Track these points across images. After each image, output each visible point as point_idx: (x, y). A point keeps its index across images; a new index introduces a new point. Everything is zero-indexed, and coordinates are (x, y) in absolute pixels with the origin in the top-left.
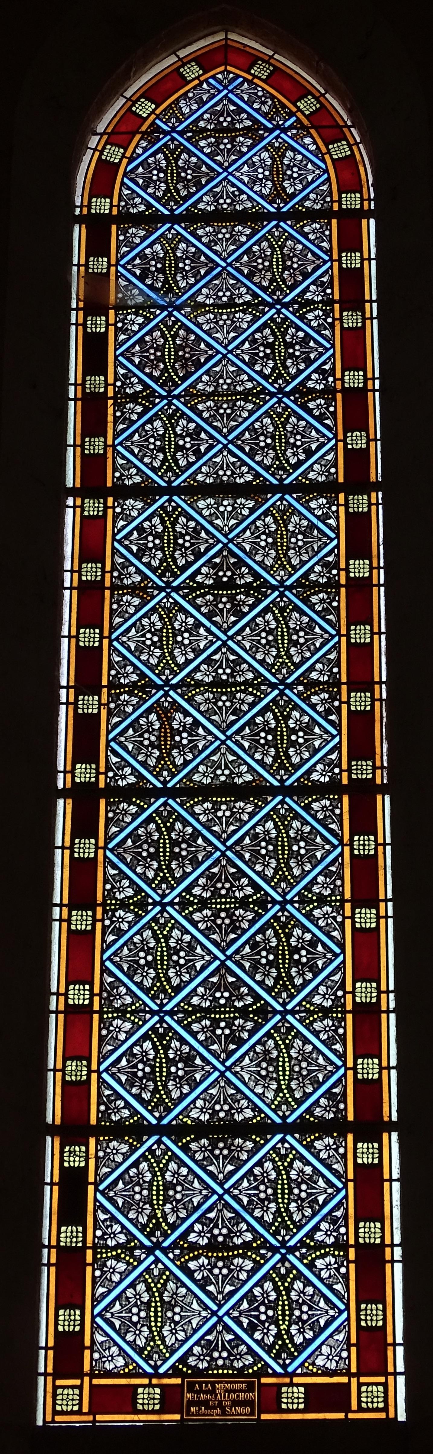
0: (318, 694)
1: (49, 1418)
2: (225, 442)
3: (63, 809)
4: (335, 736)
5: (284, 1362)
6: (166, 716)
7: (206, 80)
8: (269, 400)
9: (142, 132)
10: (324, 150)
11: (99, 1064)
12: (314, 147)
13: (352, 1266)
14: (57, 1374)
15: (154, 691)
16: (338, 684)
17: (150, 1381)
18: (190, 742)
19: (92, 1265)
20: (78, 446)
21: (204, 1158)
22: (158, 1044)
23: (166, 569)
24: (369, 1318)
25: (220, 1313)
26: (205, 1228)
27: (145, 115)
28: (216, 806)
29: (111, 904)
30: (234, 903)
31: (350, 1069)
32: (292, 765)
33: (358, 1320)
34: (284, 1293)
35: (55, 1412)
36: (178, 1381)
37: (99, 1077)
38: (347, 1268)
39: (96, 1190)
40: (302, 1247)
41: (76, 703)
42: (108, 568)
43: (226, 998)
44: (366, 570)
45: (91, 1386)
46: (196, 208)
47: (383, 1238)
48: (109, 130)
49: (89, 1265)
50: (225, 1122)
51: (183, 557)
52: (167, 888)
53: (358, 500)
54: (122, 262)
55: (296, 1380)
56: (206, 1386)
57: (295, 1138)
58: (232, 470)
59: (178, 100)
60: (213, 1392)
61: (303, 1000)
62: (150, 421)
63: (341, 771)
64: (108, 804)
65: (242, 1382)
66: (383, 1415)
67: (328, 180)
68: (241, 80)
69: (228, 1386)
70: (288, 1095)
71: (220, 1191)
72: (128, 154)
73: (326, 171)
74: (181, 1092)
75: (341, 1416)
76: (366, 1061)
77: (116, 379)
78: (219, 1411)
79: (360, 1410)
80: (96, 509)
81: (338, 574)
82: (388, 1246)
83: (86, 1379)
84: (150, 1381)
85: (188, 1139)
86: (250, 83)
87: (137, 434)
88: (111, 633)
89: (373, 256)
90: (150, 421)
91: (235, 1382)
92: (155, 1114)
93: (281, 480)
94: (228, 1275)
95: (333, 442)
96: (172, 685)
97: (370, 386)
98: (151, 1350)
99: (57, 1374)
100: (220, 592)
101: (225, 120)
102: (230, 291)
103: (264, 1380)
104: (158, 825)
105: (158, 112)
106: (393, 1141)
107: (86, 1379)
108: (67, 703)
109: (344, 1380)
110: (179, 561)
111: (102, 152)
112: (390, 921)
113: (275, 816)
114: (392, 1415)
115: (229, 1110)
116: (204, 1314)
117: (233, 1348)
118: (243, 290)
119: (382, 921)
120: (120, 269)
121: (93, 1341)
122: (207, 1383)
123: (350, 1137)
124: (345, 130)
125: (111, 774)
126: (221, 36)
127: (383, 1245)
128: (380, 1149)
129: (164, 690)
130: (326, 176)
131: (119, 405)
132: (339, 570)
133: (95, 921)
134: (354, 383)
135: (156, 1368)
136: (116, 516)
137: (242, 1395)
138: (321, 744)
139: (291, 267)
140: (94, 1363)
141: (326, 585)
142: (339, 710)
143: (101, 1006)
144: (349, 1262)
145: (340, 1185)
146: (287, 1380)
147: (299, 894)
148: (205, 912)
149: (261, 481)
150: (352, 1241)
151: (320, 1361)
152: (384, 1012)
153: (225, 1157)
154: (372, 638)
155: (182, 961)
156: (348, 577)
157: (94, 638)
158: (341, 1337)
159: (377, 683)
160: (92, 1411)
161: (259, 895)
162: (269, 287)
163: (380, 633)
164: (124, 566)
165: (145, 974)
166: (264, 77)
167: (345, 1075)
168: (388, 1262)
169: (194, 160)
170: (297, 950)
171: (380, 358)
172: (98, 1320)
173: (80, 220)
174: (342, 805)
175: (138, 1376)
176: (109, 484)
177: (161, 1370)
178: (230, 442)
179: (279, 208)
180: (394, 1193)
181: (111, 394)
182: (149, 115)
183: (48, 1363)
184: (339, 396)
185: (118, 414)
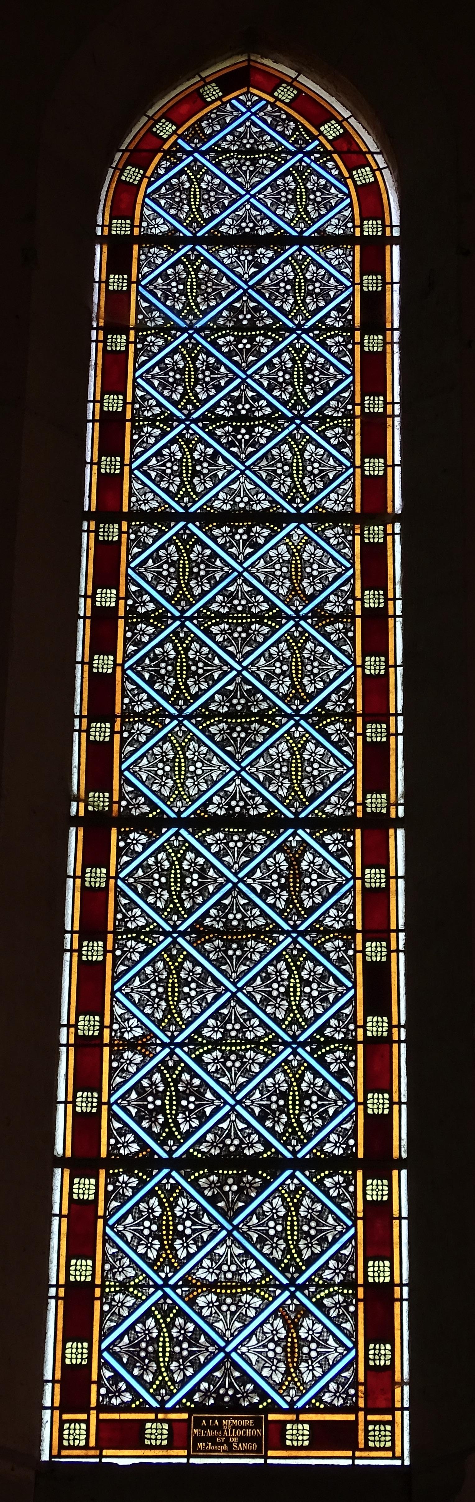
0: (334, 725)
2: (242, 468)
3: (75, 838)
4: (351, 1350)
5: (294, 1149)
7: (229, 101)
8: (289, 336)
9: (164, 151)
10: (346, 174)
11: (110, 1095)
12: (337, 172)
13: (361, 1305)
14: (64, 1408)
15: (179, 334)
16: (352, 330)
17: (156, 1416)
19: (100, 1298)
20: (100, 341)
21: (224, 640)
23: (190, 310)
25: (228, 1349)
26: (214, 1264)
27: (165, 136)
28: (229, 836)
29: (110, 1286)
31: (361, 1104)
32: (305, 1020)
33: (367, 1359)
36: (185, 1416)
37: (110, 1109)
38: (356, 1306)
39: (105, 1224)
40: (312, 932)
42: (129, 399)
43: (238, 920)
45: (99, 1421)
46: (208, 610)
48: (132, 147)
49: (97, 1299)
50: (235, 1157)
52: (189, 502)
54: (122, 875)
55: (303, 1417)
56: (213, 1422)
59: (201, 120)
60: (220, 1428)
63: (356, 804)
64: (107, 1175)
65: (249, 1419)
67: (351, 205)
68: (263, 102)
69: (235, 1422)
70: (298, 1016)
71: (232, 1102)
72: (148, 174)
73: (349, 196)
74: (185, 1374)
78: (225, 1447)
81: (354, 604)
83: (93, 1413)
84: (156, 1416)
85: (204, 832)
86: (273, 105)
88: (124, 662)
91: (242, 1418)
93: (294, 1153)
95: (353, 1106)
96: (177, 1043)
97: (389, 411)
99: (64, 1408)
100: (231, 830)
102: (248, 496)
103: (272, 1417)
104: (189, 177)
106: (401, 1178)
107: (93, 1413)
109: (352, 1417)
110: (191, 688)
112: (405, 1304)
117: (245, 1021)
118: (262, 496)
119: (396, 1108)
120: (120, 883)
121: (100, 1376)
122: (214, 1419)
123: (360, 1174)
124: (369, 156)
129: (172, 937)
130: (348, 201)
131: (116, 1054)
132: (355, 599)
135: (163, 1403)
136: (136, 351)
137: (249, 1432)
139: (312, 380)
141: (343, 1041)
143: (111, 1038)
144: (358, 1300)
145: (350, 1223)
149: (272, 1153)
150: (361, 1281)
151: (327, 1398)
152: (392, 715)
153: (233, 1314)
154: (385, 471)
155: (192, 1106)
156: (363, 608)
159: (391, 616)
161: (269, 1153)
162: (289, 401)
163: (400, 1103)
164: (122, 1133)
165: (156, 1006)
166: (287, 101)
167: (356, 1110)
168: (397, 1300)
169: (201, 861)
170: (307, 1096)
172: (106, 1355)
176: (125, 509)
177: (169, 1405)
178: (248, 468)
180: (402, 1232)
181: (106, 1039)
182: (170, 137)
183: (59, 1311)
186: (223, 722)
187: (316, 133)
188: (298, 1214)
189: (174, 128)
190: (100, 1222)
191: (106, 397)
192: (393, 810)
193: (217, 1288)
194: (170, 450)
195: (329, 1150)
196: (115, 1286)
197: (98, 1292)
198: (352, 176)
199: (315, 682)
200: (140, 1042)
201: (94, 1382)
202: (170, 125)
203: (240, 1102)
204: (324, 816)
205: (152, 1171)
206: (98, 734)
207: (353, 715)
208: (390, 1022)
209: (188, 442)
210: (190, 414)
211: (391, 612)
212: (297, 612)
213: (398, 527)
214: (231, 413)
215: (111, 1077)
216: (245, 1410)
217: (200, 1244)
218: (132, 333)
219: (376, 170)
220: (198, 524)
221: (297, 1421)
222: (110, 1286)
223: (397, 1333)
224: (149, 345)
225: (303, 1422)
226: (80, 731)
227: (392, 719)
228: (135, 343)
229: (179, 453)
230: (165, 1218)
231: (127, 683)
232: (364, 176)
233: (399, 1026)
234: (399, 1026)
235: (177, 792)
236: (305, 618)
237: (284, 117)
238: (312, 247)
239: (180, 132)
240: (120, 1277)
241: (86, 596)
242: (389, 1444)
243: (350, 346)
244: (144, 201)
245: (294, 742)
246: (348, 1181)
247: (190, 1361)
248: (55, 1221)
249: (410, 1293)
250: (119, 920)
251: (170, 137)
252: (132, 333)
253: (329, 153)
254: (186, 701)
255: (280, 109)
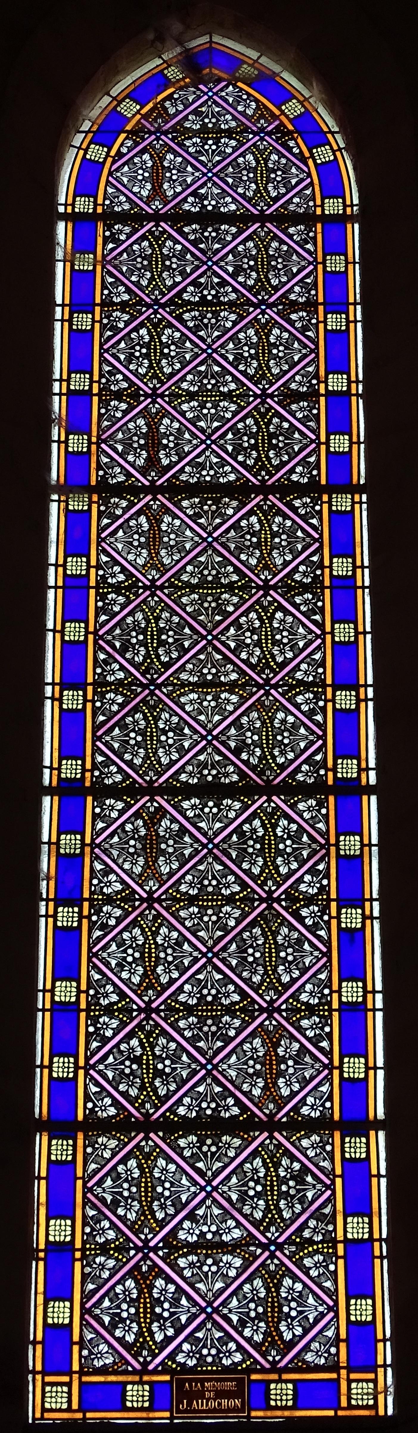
1: (38, 1415)
6: (155, 519)
9: (127, 132)
10: (307, 154)
13: (341, 1262)
15: (144, 309)
16: (316, 304)
18: (178, 266)
22: (144, 1041)
24: (344, 770)
29: (90, 1249)
30: (220, 1010)
34: (273, 1290)
35: (44, 1410)
36: (167, 1378)
41: (70, 321)
42: (88, 766)
44: (348, 504)
45: (81, 1384)
47: (371, 1232)
48: (95, 128)
51: (170, 365)
53: (347, 764)
55: (285, 1376)
56: (196, 1385)
57: (282, 1135)
58: (217, 989)
59: (164, 100)
61: (286, 675)
62: (136, 329)
66: (372, 1413)
72: (113, 153)
73: (309, 175)
75: (331, 1413)
76: (348, 838)
77: (101, 376)
79: (350, 1407)
80: (77, 634)
81: (326, 775)
82: (377, 1240)
83: (75, 1377)
87: (121, 531)
89: (362, 439)
90: (136, 329)
92: (144, 998)
94: (216, 1152)
98: (142, 1224)
101: (209, 319)
103: (254, 1377)
104: (145, 715)
105: (143, 112)
107: (75, 1377)
108: (62, 320)
109: (334, 1376)
111: (86, 151)
113: (262, 815)
114: (381, 1412)
115: (217, 885)
116: (193, 1189)
123: (337, 1135)
124: (329, 136)
125: (92, 992)
126: (205, 39)
127: (371, 1240)
128: (371, 1224)
130: (309, 180)
131: (104, 403)
133: (81, 917)
134: (347, 764)
136: (100, 514)
138: (311, 961)
140: (83, 1360)
142: (324, 710)
144: (338, 1257)
146: (275, 1377)
147: (285, 892)
148: (190, 1020)
150: (340, 1236)
157: (79, 632)
158: (330, 1333)
160: (82, 1409)
163: (363, 567)
165: (128, 1207)
171: (372, 622)
173: (65, 217)
174: (333, 1140)
175: (126, 1372)
177: (151, 1367)
179: (271, 1137)
181: (95, 390)
182: (134, 116)
184: (322, 400)
185: (103, 411)
186: (195, 310)
187: (277, 112)
188: (271, 625)
189: (138, 107)
190: (79, 1183)
191: (64, 762)
192: (364, 776)
193: (199, 396)
194: (138, 333)
195: (306, 1113)
196: (95, 1249)
197: (78, 1255)
198: (312, 156)
199: (286, 752)
200: (113, 1245)
201: (76, 1343)
202: (134, 105)
203: (216, 955)
204: (294, 682)
205: (138, 591)
206: (70, 702)
207: (316, 304)
208: (356, 628)
209: (155, 376)
210: (151, 1001)
211: (370, 1006)
212: (264, 390)
213: (364, 498)
214: (198, 126)
215: (83, 1283)
216: (226, 1370)
217: (184, 187)
218: (90, 689)
219: (337, 150)
220: (161, 1134)
221: (280, 1381)
222: (103, 588)
223: (358, 551)
224: (115, 321)
225: (287, 1381)
226: (47, 916)
227: (351, 308)
228: (93, 702)
229: (141, 938)
230: (147, 946)
231: (93, 972)
232: (324, 154)
233: (357, 382)
234: (357, 382)
235: (149, 762)
236: (272, 396)
237: (245, 97)
238: (282, 797)
239: (143, 112)
240: (101, 1240)
241: (44, 991)
242: (371, 1402)
243: (321, 703)
244: (108, 181)
245: (259, 153)
246: (320, 804)
247: (174, 965)
248: (51, 594)
249: (385, 1001)
250: (87, 1234)
251: (134, 116)
252: (90, 689)
253: (290, 132)
254: (151, 1351)
255: (241, 90)
